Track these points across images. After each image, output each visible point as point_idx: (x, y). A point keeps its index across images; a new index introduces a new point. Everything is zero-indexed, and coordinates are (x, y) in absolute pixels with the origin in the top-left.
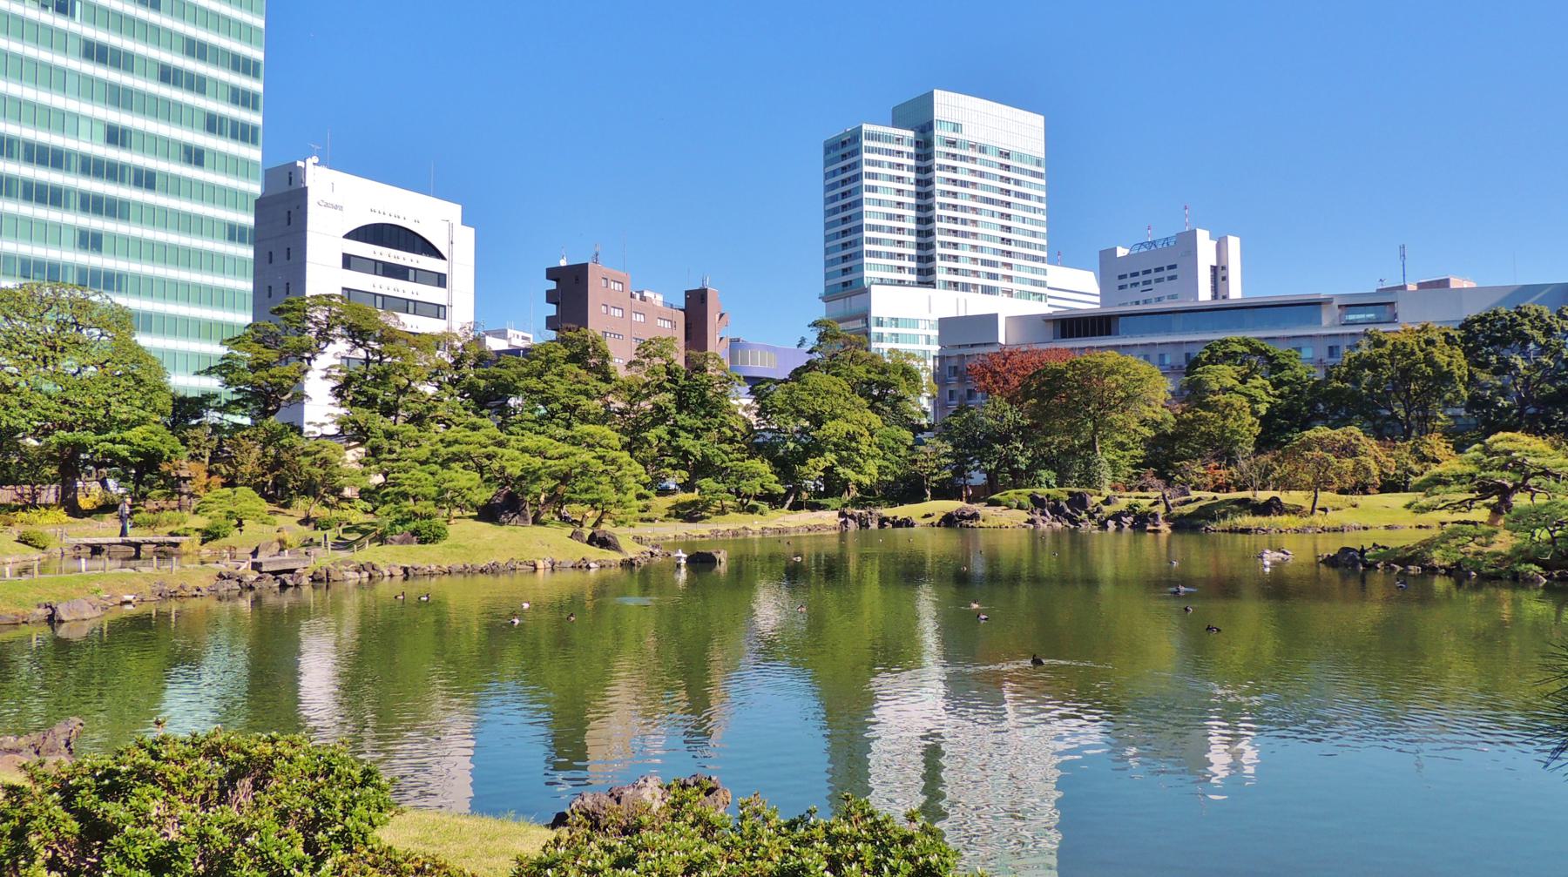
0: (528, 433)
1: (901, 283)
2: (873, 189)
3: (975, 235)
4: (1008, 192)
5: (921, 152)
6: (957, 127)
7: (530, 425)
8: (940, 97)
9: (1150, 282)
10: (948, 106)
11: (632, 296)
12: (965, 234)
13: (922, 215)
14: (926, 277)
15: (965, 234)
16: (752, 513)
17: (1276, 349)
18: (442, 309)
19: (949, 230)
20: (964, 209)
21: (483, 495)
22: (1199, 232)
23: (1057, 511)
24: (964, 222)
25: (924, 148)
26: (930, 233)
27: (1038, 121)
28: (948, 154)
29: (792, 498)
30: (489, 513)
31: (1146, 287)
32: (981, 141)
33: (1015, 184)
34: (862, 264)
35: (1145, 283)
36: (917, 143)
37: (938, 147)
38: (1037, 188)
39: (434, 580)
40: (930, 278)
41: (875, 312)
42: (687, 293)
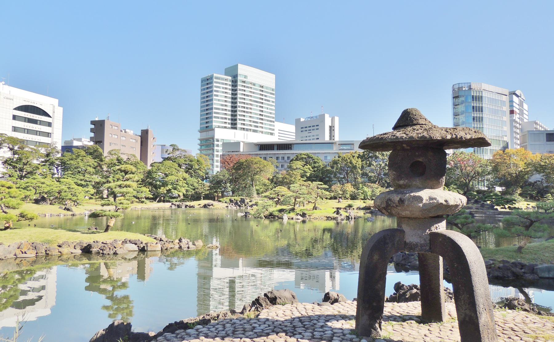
0: (69, 178)
1: (225, 127)
2: (217, 96)
3: (251, 113)
4: (262, 99)
5: (233, 84)
6: (246, 77)
7: (71, 175)
8: (240, 67)
9: (310, 130)
10: (243, 70)
12: (247, 112)
13: (233, 105)
14: (234, 126)
15: (247, 112)
16: (142, 203)
18: (49, 134)
19: (242, 111)
20: (247, 104)
21: (37, 196)
22: (326, 115)
23: (236, 204)
24: (247, 108)
25: (234, 83)
26: (236, 111)
27: (273, 76)
28: (242, 85)
29: (158, 199)
30: (37, 202)
32: (254, 82)
33: (265, 96)
34: (212, 121)
35: (309, 130)
36: (232, 81)
37: (239, 83)
38: (272, 98)
40: (235, 126)
41: (216, 137)
42: (142, 130)
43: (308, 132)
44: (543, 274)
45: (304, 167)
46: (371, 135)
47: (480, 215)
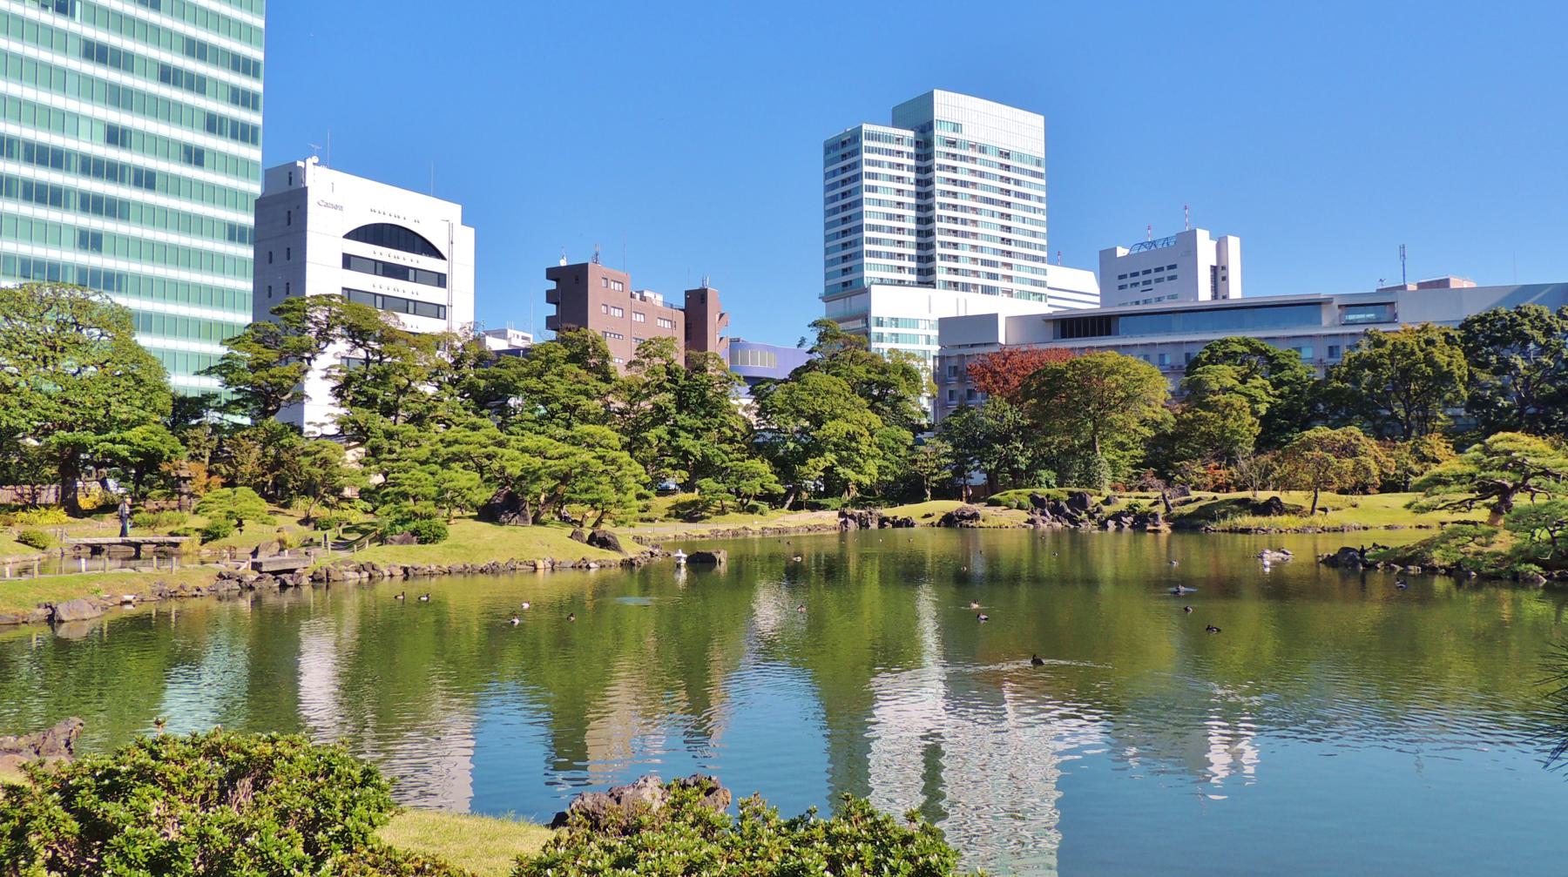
0: (528, 433)
1: (901, 283)
2: (873, 189)
3: (975, 235)
4: (1008, 192)
5: (921, 152)
6: (957, 127)
7: (530, 425)
8: (940, 97)
9: (1150, 282)
10: (948, 106)
12: (965, 234)
13: (922, 215)
14: (926, 277)
15: (965, 234)
16: (752, 513)
18: (442, 309)
19: (949, 230)
20: (964, 209)
21: (483, 495)
22: (1199, 232)
23: (1057, 511)
24: (964, 222)
25: (924, 148)
26: (930, 233)
27: (1038, 121)
28: (948, 154)
30: (489, 513)
31: (1146, 287)
32: (981, 141)
33: (1015, 184)
34: (862, 264)
35: (1145, 283)
36: (917, 143)
37: (938, 147)
38: (1037, 188)
39: (434, 580)
40: (930, 278)
41: (875, 312)
42: (687, 293)
45: (1248, 385)
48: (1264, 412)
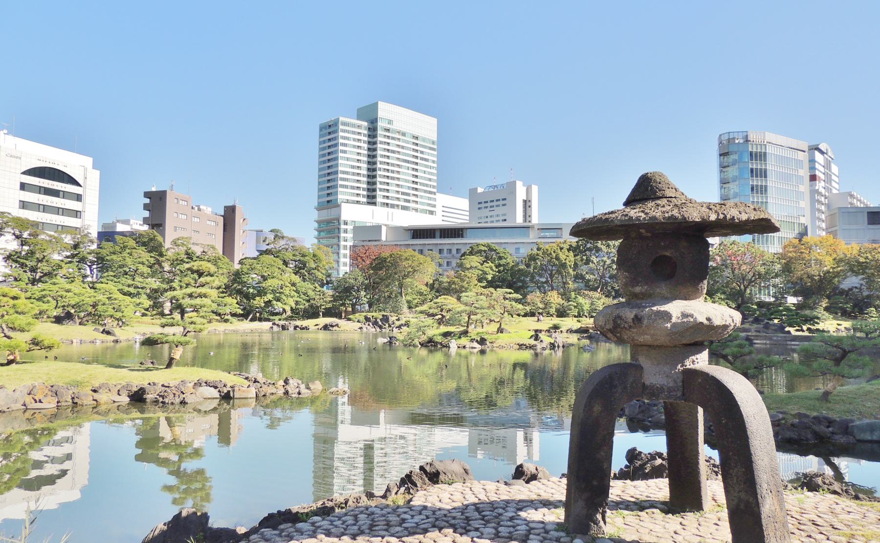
0: (110, 282)
1: (358, 202)
2: (345, 152)
3: (398, 179)
4: (417, 157)
5: (371, 133)
6: (390, 122)
7: (112, 278)
8: (382, 106)
9: (493, 206)
10: (386, 111)
11: (192, 208)
12: (393, 178)
13: (370, 167)
14: (371, 199)
15: (393, 178)
16: (226, 322)
17: (500, 249)
18: (79, 213)
19: (384, 176)
20: (393, 165)
21: (58, 312)
22: (518, 182)
23: (375, 323)
24: (393, 172)
25: (372, 132)
26: (374, 177)
27: (434, 121)
28: (385, 136)
29: (251, 315)
30: (58, 320)
32: (403, 130)
33: (421, 153)
34: (337, 191)
35: (491, 207)
36: (369, 128)
37: (380, 132)
38: (432, 156)
40: (373, 201)
41: (344, 217)
42: (225, 207)
43: (489, 209)
44: (862, 435)
46: (589, 215)
47: (762, 342)
48: (490, 279)
